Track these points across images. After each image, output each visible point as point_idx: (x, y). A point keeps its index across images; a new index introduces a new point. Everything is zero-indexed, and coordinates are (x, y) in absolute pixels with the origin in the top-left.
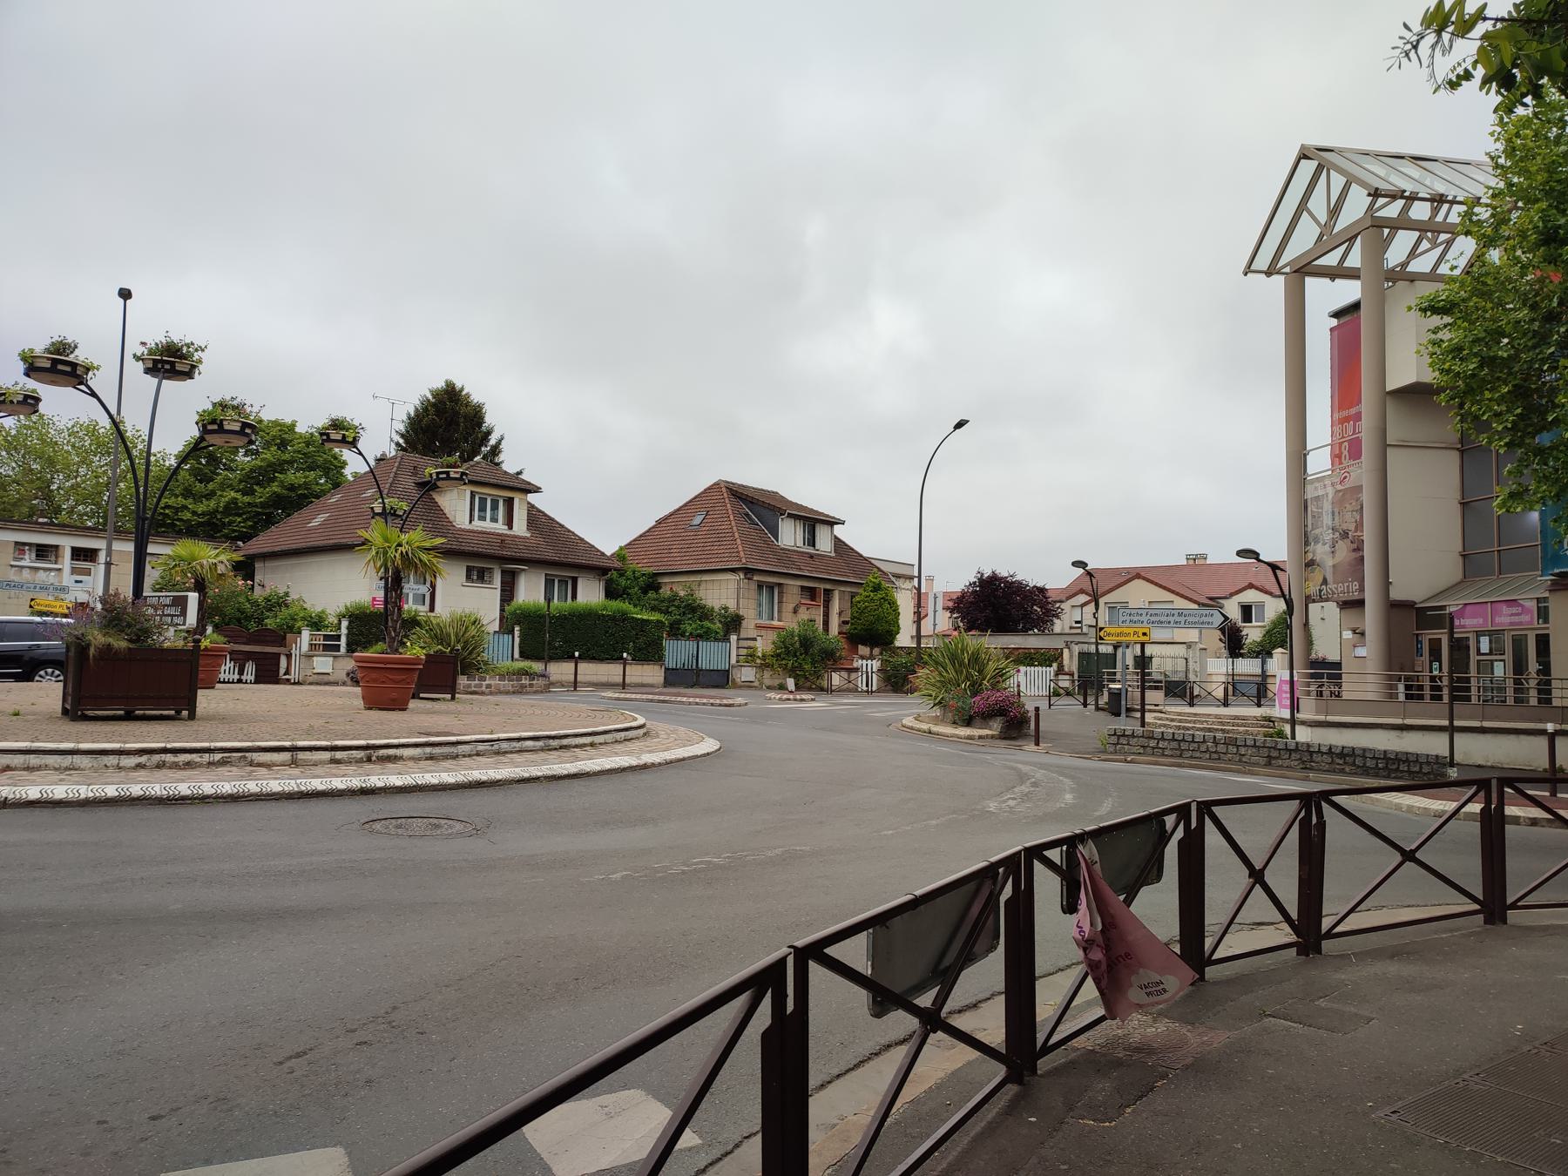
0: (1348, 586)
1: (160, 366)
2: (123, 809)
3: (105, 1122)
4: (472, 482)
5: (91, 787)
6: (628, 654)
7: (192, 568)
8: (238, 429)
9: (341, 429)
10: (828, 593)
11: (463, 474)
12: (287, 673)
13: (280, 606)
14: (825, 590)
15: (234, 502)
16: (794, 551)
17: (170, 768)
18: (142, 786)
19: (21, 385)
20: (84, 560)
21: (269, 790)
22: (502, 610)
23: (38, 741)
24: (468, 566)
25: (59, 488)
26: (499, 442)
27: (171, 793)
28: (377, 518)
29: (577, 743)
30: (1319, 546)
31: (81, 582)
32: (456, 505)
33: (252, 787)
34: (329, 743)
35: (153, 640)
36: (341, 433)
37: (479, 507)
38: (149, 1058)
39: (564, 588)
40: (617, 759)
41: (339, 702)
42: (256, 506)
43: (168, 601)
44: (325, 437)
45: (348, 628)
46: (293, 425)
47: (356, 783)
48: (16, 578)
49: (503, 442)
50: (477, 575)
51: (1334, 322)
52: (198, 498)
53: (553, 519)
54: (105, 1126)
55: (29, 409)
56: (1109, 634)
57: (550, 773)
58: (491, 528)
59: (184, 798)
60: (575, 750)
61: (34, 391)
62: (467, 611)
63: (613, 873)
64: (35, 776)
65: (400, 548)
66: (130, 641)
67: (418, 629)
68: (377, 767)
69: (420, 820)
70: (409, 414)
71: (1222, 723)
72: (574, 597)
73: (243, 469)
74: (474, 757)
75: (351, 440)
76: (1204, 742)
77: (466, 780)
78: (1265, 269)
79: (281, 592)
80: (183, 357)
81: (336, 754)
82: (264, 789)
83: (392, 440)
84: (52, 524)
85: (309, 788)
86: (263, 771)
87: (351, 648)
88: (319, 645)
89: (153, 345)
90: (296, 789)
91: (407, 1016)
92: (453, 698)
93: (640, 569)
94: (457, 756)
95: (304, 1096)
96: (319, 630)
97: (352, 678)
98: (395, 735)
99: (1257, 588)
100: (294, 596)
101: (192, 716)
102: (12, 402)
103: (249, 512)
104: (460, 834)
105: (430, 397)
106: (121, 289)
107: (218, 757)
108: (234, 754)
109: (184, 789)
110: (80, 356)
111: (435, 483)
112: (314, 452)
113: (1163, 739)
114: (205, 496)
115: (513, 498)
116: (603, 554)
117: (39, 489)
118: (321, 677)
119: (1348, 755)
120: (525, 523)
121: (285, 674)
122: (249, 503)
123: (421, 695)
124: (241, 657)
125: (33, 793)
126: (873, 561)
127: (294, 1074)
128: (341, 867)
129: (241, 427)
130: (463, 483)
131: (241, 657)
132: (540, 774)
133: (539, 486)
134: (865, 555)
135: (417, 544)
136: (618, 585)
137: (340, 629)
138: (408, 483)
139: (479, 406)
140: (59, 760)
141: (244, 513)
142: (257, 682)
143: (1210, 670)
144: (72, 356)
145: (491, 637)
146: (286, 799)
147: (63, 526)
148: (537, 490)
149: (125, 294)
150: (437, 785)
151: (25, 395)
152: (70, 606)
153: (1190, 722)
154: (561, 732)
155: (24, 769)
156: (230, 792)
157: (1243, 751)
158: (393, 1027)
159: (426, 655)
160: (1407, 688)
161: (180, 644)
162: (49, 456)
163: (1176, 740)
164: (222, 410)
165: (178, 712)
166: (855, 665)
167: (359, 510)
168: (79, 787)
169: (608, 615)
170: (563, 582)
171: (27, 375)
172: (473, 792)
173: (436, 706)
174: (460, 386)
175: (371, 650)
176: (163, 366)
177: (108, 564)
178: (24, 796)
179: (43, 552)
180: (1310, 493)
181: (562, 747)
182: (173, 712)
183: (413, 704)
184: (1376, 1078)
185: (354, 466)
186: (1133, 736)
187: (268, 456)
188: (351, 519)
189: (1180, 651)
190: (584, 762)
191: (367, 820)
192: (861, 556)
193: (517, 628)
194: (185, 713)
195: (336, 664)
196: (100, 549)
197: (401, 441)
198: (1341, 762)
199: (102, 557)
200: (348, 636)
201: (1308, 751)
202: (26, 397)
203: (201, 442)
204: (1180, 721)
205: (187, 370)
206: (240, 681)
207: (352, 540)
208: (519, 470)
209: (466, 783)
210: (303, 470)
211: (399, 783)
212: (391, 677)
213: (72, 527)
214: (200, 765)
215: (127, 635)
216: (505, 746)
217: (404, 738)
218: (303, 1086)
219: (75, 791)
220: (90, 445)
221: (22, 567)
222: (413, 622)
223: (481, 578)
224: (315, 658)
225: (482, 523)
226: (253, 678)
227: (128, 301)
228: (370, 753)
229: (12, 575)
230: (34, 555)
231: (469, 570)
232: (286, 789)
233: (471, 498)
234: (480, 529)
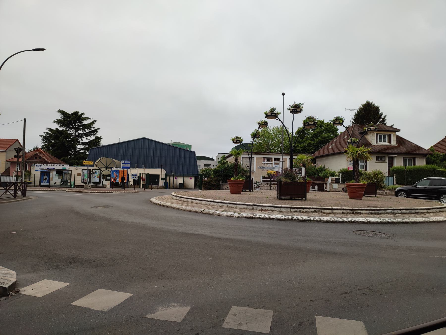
1: (294, 110)
2: (293, 222)
3: (300, 299)
4: (379, 131)
5: (285, 216)
7: (302, 161)
8: (313, 124)
9: (338, 120)
11: (375, 128)
12: (326, 188)
13: (323, 170)
15: (310, 143)
17: (302, 212)
19: (264, 120)
20: (277, 161)
21: (327, 220)
22: (389, 169)
23: (273, 204)
25: (271, 144)
26: (385, 117)
27: (303, 219)
28: (349, 144)
29: (421, 212)
31: (277, 166)
32: (372, 139)
33: (322, 219)
34: (341, 208)
35: (296, 180)
36: (339, 121)
37: (380, 138)
38: (308, 285)
39: (410, 161)
40: (438, 218)
41: (342, 197)
42: (315, 144)
43: (298, 170)
44: (334, 123)
45: (341, 176)
46: (324, 121)
47: (350, 219)
48: (263, 166)
49: (386, 117)
50: (380, 159)
52: (301, 143)
53: (405, 140)
54: (300, 300)
55: (265, 126)
57: (412, 221)
58: (384, 144)
59: (306, 220)
60: (421, 214)
61: (267, 121)
62: (377, 170)
63: (442, 256)
64: (273, 212)
65: (358, 152)
66: (291, 180)
67: (362, 176)
68: (356, 216)
69: (370, 232)
70: (356, 113)
72: (415, 164)
73: (312, 134)
74: (385, 214)
75: (341, 123)
77: (384, 221)
79: (323, 166)
80: (299, 107)
81: (344, 212)
82: (326, 220)
83: (351, 121)
84: (270, 153)
85: (337, 220)
86: (325, 215)
87: (343, 182)
88: (334, 181)
89: (292, 105)
90: (334, 220)
91: (376, 289)
92: (376, 196)
93: (440, 153)
94: (380, 214)
95: (349, 305)
96: (334, 177)
97: (344, 190)
98: (360, 207)
100: (326, 167)
101: (306, 199)
102: (262, 124)
103: (313, 146)
104: (384, 237)
105: (362, 107)
106: (282, 93)
107: (313, 210)
108: (317, 210)
109: (306, 218)
110: (276, 111)
111: (367, 132)
112: (329, 127)
114: (302, 143)
115: (391, 134)
116: (425, 149)
117: (267, 145)
118: (335, 190)
120: (395, 142)
121: (325, 189)
122: (313, 143)
123: (366, 195)
124: (314, 184)
125: (273, 217)
127: (346, 298)
128: (349, 243)
129: (314, 123)
130: (375, 131)
131: (314, 184)
132: (409, 221)
133: (400, 129)
135: (363, 151)
136: (431, 159)
137: (339, 176)
138: (357, 133)
139: (378, 107)
141: (312, 146)
142: (318, 191)
144: (275, 111)
145: (386, 178)
146: (331, 222)
147: (272, 153)
148: (399, 130)
149: (283, 94)
150: (375, 222)
151: (265, 122)
152: (275, 172)
155: (271, 211)
156: (317, 219)
158: (372, 291)
159: (367, 183)
161: (302, 181)
162: (268, 136)
164: (309, 119)
165: (302, 198)
168: (283, 216)
169: (428, 170)
170: (410, 160)
171: (266, 118)
172: (386, 225)
173: (371, 198)
174: (371, 102)
175: (350, 182)
176: (294, 110)
177: (282, 161)
178: (272, 217)
179: (269, 159)
181: (416, 213)
182: (301, 198)
183: (363, 198)
185: (341, 129)
187: (318, 130)
188: (341, 145)
191: (354, 230)
193: (395, 175)
194: (304, 199)
195: (339, 186)
196: (280, 158)
197: (354, 121)
199: (281, 160)
200: (342, 178)
202: (265, 123)
203: (304, 128)
205: (300, 110)
206: (314, 191)
207: (341, 151)
208: (392, 125)
209: (384, 222)
210: (327, 133)
211: (363, 220)
213: (274, 153)
214: (309, 212)
215: (290, 179)
216: (396, 211)
217: (363, 207)
218: (349, 302)
220: (277, 133)
221: (265, 163)
222: (361, 174)
224: (333, 185)
226: (317, 190)
227: (284, 96)
228: (353, 211)
229: (263, 165)
230: (267, 160)
232: (331, 220)
233: (377, 135)
234: (380, 145)
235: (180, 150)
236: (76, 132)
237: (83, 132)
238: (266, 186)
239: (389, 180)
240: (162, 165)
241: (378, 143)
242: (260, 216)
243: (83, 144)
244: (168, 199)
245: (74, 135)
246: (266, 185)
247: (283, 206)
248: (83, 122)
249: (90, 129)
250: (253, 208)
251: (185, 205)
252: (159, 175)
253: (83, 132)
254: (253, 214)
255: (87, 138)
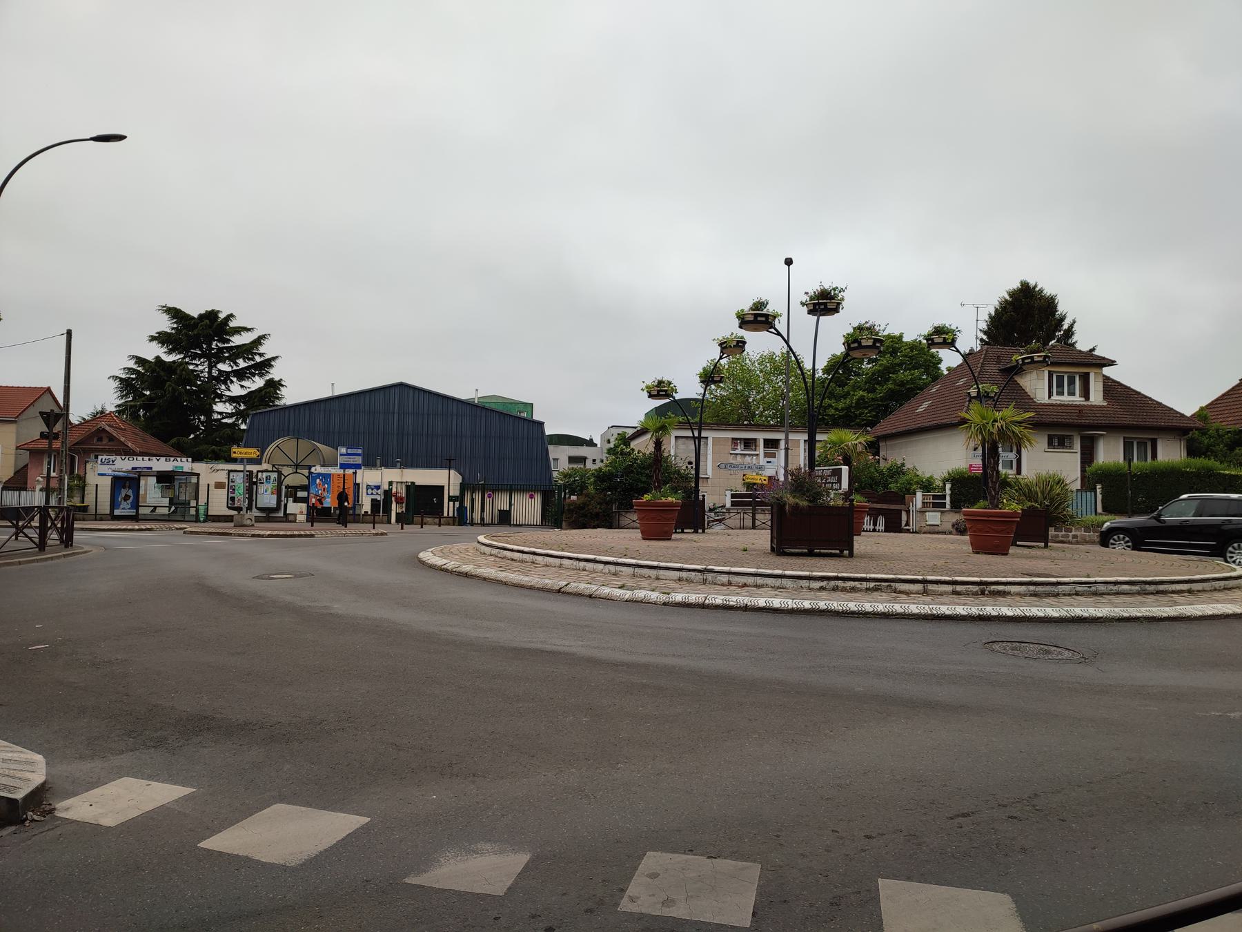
1: (817, 307)
2: (815, 617)
3: (837, 832)
4: (1054, 364)
5: (795, 601)
7: (841, 448)
8: (871, 344)
9: (942, 334)
11: (1046, 357)
12: (907, 524)
13: (899, 474)
15: (862, 398)
17: (842, 591)
19: (734, 335)
20: (772, 448)
21: (910, 611)
22: (1083, 471)
23: (761, 568)
25: (754, 400)
26: (1071, 326)
27: (844, 609)
28: (973, 400)
29: (1174, 589)
31: (770, 462)
32: (1037, 386)
33: (898, 608)
34: (951, 579)
35: (823, 500)
36: (943, 337)
37: (1057, 384)
38: (858, 793)
39: (1143, 448)
40: (1219, 606)
41: (952, 547)
42: (877, 400)
43: (829, 473)
44: (930, 342)
45: (951, 489)
46: (901, 336)
47: (974, 611)
48: (734, 462)
49: (1075, 326)
50: (1058, 442)
52: (838, 398)
53: (1129, 388)
54: (837, 834)
55: (739, 350)
57: (1148, 614)
58: (1069, 401)
59: (853, 613)
60: (1173, 595)
61: (742, 337)
62: (1051, 473)
63: (1230, 712)
64: (761, 591)
65: (996, 424)
66: (809, 501)
67: (1008, 489)
68: (990, 600)
69: (1031, 645)
70: (990, 314)
72: (1154, 456)
73: (868, 374)
74: (1073, 596)
75: (950, 341)
77: (1068, 615)
79: (899, 462)
80: (832, 298)
81: (957, 589)
82: (907, 611)
83: (977, 338)
84: (751, 425)
85: (939, 613)
86: (904, 597)
87: (956, 505)
88: (930, 503)
89: (813, 293)
90: (929, 612)
91: (1048, 803)
92: (1046, 546)
93: (1225, 427)
94: (1058, 595)
95: (973, 848)
96: (929, 492)
97: (957, 529)
98: (1002, 575)
100: (908, 466)
101: (851, 555)
102: (730, 346)
103: (872, 405)
104: (1069, 661)
105: (1008, 298)
106: (786, 259)
107: (872, 584)
108: (883, 584)
109: (852, 606)
110: (770, 309)
111: (1021, 368)
112: (917, 354)
114: (842, 397)
115: (1089, 373)
116: (1183, 415)
117: (742, 402)
118: (932, 527)
120: (1101, 394)
121: (906, 526)
122: (873, 399)
123: (1018, 543)
124: (874, 512)
125: (762, 602)
127: (963, 829)
128: (973, 676)
129: (873, 342)
130: (1045, 365)
131: (874, 512)
132: (1139, 615)
133: (1113, 359)
135: (1010, 419)
136: (1200, 443)
137: (945, 490)
138: (993, 369)
139: (1052, 297)
141: (869, 406)
142: (886, 530)
144: (765, 310)
145: (1074, 495)
146: (923, 619)
147: (758, 425)
148: (1111, 363)
149: (789, 262)
150: (1043, 618)
151: (737, 341)
152: (766, 478)
155: (754, 586)
156: (883, 610)
158: (1037, 810)
159: (1022, 509)
161: (840, 503)
162: (747, 380)
164: (860, 332)
165: (842, 552)
168: (787, 600)
169: (1192, 472)
170: (1142, 444)
171: (741, 327)
172: (1076, 626)
173: (1033, 552)
174: (1034, 284)
175: (976, 506)
176: (819, 307)
177: (787, 449)
178: (757, 604)
179: (749, 443)
181: (1158, 592)
182: (838, 552)
183: (1012, 550)
184: (484, 927)
185: (949, 359)
187: (884, 362)
188: (949, 404)
191: (987, 641)
193: (1099, 487)
194: (846, 552)
195: (944, 517)
196: (780, 440)
197: (985, 337)
199: (782, 444)
200: (951, 495)
202: (738, 342)
203: (847, 357)
205: (835, 307)
206: (874, 530)
207: (951, 420)
208: (1092, 347)
209: (1069, 618)
210: (910, 369)
211: (1010, 613)
213: (764, 426)
214: (860, 590)
215: (807, 497)
216: (1102, 588)
217: (1010, 577)
218: (971, 840)
220: (771, 369)
221: (737, 454)
222: (1005, 483)
224: (927, 514)
226: (883, 528)
227: (791, 266)
228: (984, 588)
229: (731, 460)
230: (742, 446)
232: (922, 612)
233: (1049, 377)
234: (1058, 403)
235: (502, 418)
236: (210, 368)
237: (232, 368)
238: (742, 517)
239: (1084, 502)
240: (450, 460)
241: (1052, 398)
242: (725, 602)
243: (232, 400)
244: (468, 555)
245: (207, 376)
246: (742, 514)
247: (788, 573)
248: (231, 338)
249: (249, 359)
250: (705, 577)
251: (516, 569)
252: (444, 486)
253: (232, 368)
254: (704, 595)
255: (241, 383)
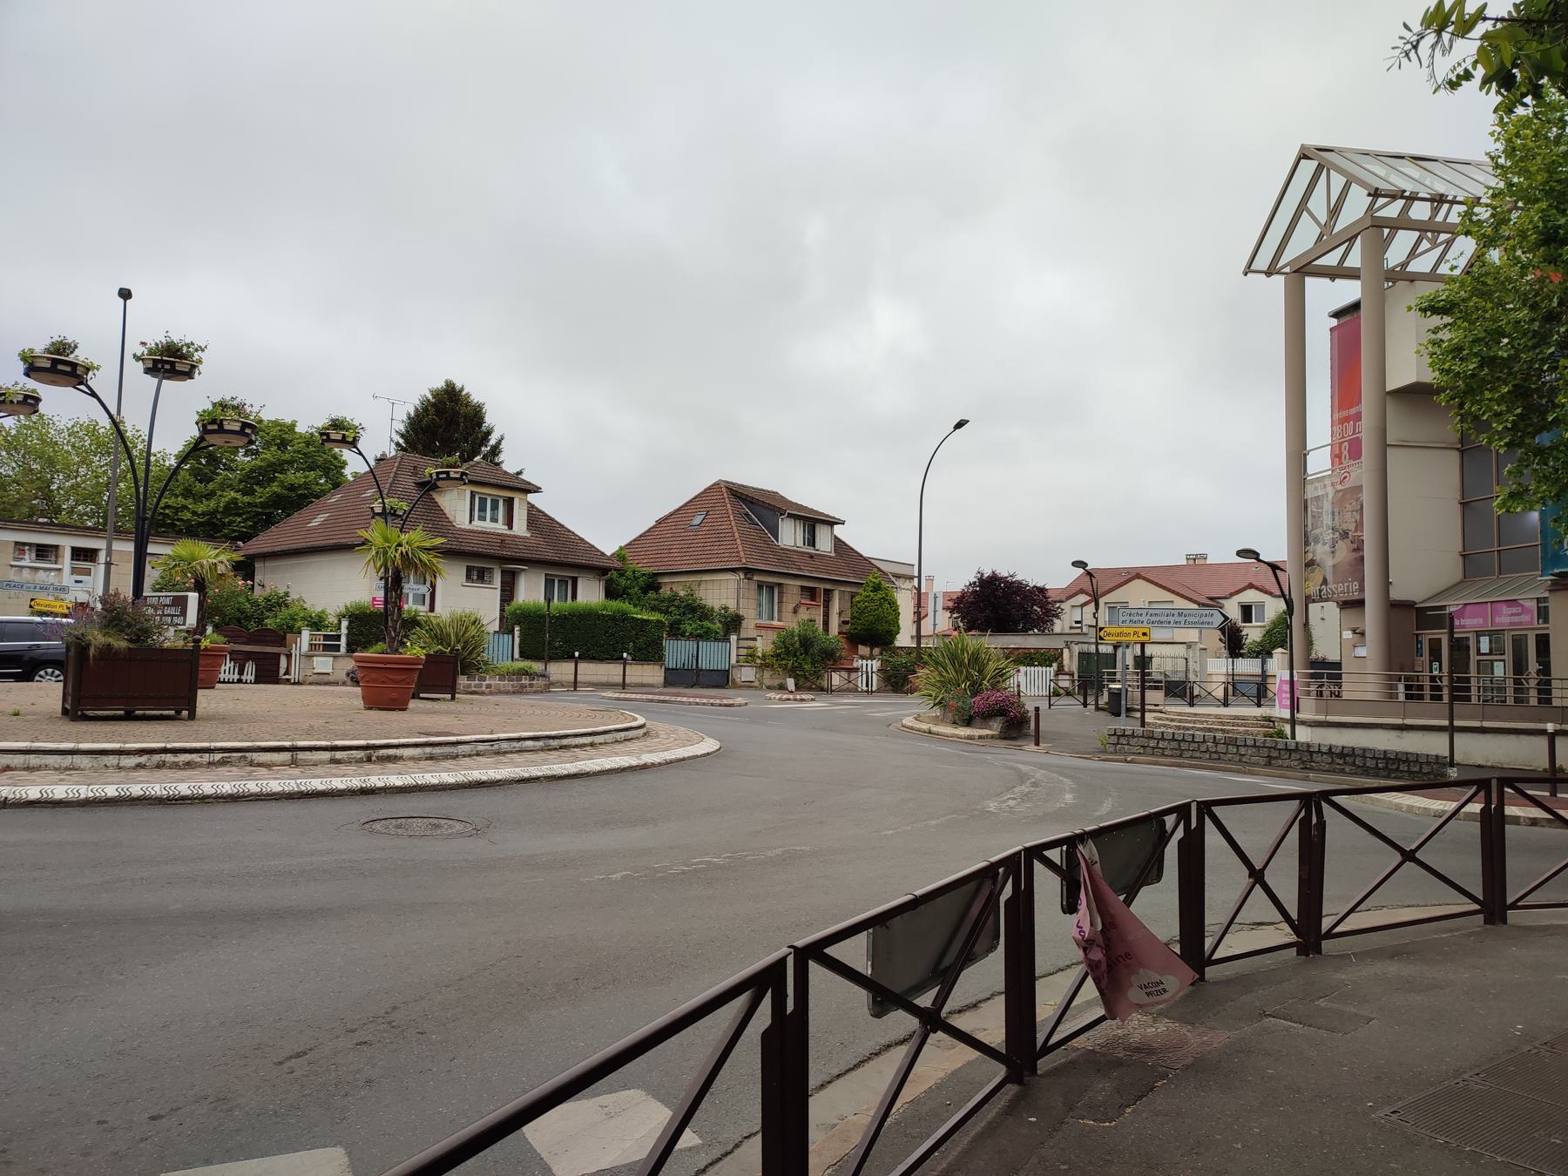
0: (1348, 586)
1: (160, 366)
2: (123, 809)
3: (105, 1122)
4: (472, 482)
5: (91, 787)
6: (628, 654)
7: (192, 568)
8: (238, 429)
9: (341, 429)
10: (828, 593)
11: (463, 474)
12: (287, 673)
13: (280, 606)
14: (825, 590)
15: (234, 502)
16: (794, 551)
17: (170, 768)
18: (142, 786)
19: (21, 385)
20: (84, 560)
21: (269, 790)
22: (502, 610)
23: (38, 741)
24: (468, 566)
25: (59, 488)
26: (499, 442)
27: (171, 793)
28: (377, 518)
29: (577, 743)
30: (1319, 546)
31: (81, 582)
32: (456, 505)
33: (252, 787)
34: (329, 743)
35: (153, 640)
36: (341, 433)
37: (479, 507)
38: (149, 1058)
39: (564, 588)
40: (617, 759)
41: (339, 702)
42: (256, 506)
43: (168, 601)
44: (325, 437)
45: (348, 628)
46: (293, 425)
47: (356, 783)
48: (16, 578)
49: (503, 442)
50: (477, 575)
51: (1334, 322)
52: (198, 498)
53: (553, 519)
54: (105, 1126)
55: (29, 409)
56: (1109, 634)
57: (550, 773)
58: (491, 528)
59: (184, 798)
60: (575, 750)
61: (34, 391)
62: (467, 611)
63: (613, 873)
64: (35, 776)
65: (400, 548)
66: (130, 641)
67: (418, 629)
68: (377, 767)
69: (420, 820)
70: (409, 414)
71: (1222, 723)
72: (574, 597)
73: (243, 469)
74: (474, 757)
75: (351, 440)
76: (1204, 742)
77: (466, 780)
78: (1265, 269)
79: (281, 592)
80: (183, 357)
81: (336, 754)
82: (264, 789)
83: (392, 440)
84: (52, 524)
85: (309, 788)
86: (263, 771)
87: (351, 648)
88: (319, 645)
89: (153, 345)
90: (296, 789)
91: (407, 1016)
92: (453, 698)
93: (640, 569)
94: (457, 756)
95: (304, 1096)
96: (319, 630)
97: (352, 678)
98: (395, 735)
99: (1257, 588)
100: (294, 596)
101: (192, 716)
102: (12, 402)
103: (249, 512)
104: (460, 834)
105: (430, 397)
106: (121, 289)
107: (218, 757)
108: (234, 754)
109: (184, 789)
110: (80, 356)
111: (435, 483)
112: (314, 452)
113: (1163, 739)
114: (205, 496)
115: (513, 498)
116: (603, 554)
117: (39, 489)
118: (321, 677)
119: (1348, 755)
120: (525, 523)
121: (285, 674)
122: (249, 503)
123: (421, 695)
124: (241, 657)
125: (33, 793)
126: (873, 561)
127: (294, 1074)
128: (341, 867)
129: (241, 427)
130: (463, 483)
131: (241, 657)
132: (540, 774)
133: (539, 486)
134: (865, 555)
135: (417, 544)
136: (618, 585)
137: (340, 629)
138: (408, 483)
139: (479, 406)
140: (59, 760)
141: (244, 513)
142: (257, 682)
143: (1210, 670)
144: (72, 356)
145: (491, 637)
146: (286, 799)
147: (63, 526)
148: (537, 490)
149: (125, 294)
150: (437, 785)
151: (25, 395)
152: (70, 606)
153: (1190, 722)
154: (561, 732)
155: (24, 769)
156: (230, 792)
157: (1243, 751)
158: (393, 1027)
159: (426, 655)
160: (1407, 688)
161: (180, 644)
162: (49, 456)
163: (1176, 740)
164: (222, 410)
165: (178, 712)
166: (855, 665)
167: (359, 510)
168: (79, 787)
169: (608, 615)
170: (563, 582)
171: (27, 375)
172: (473, 792)
173: (436, 706)
174: (460, 386)
175: (371, 650)
176: (163, 366)
177: (108, 564)
178: (24, 796)
179: (43, 552)
180: (1310, 493)
181: (562, 747)
182: (173, 712)
183: (413, 704)
185: (354, 466)
186: (1133, 736)
187: (268, 456)
188: (351, 519)
189: (1180, 651)
190: (584, 762)
191: (367, 820)
192: (861, 556)
193: (517, 628)
194: (185, 713)
195: (336, 664)
196: (100, 549)
197: (401, 441)
198: (1341, 762)
199: (102, 557)
200: (348, 636)
201: (1308, 751)
202: (26, 397)
203: (201, 442)
204: (1180, 721)
205: (187, 370)
206: (240, 681)
207: (352, 540)
208: (519, 470)
209: (466, 783)
210: (303, 470)
211: (399, 783)
212: (391, 677)
213: (72, 527)
214: (200, 765)
215: (127, 635)
216: (505, 746)
217: (404, 738)
218: (303, 1086)
219: (75, 791)
220: (90, 445)
221: (22, 567)
222: (413, 622)
223: (481, 578)
224: (315, 658)
225: (482, 523)
226: (253, 678)
227: (128, 301)
228: (370, 753)
229: (12, 575)
230: (34, 555)
231: (469, 570)
232: (286, 789)
233: (471, 498)
234: (480, 529)
